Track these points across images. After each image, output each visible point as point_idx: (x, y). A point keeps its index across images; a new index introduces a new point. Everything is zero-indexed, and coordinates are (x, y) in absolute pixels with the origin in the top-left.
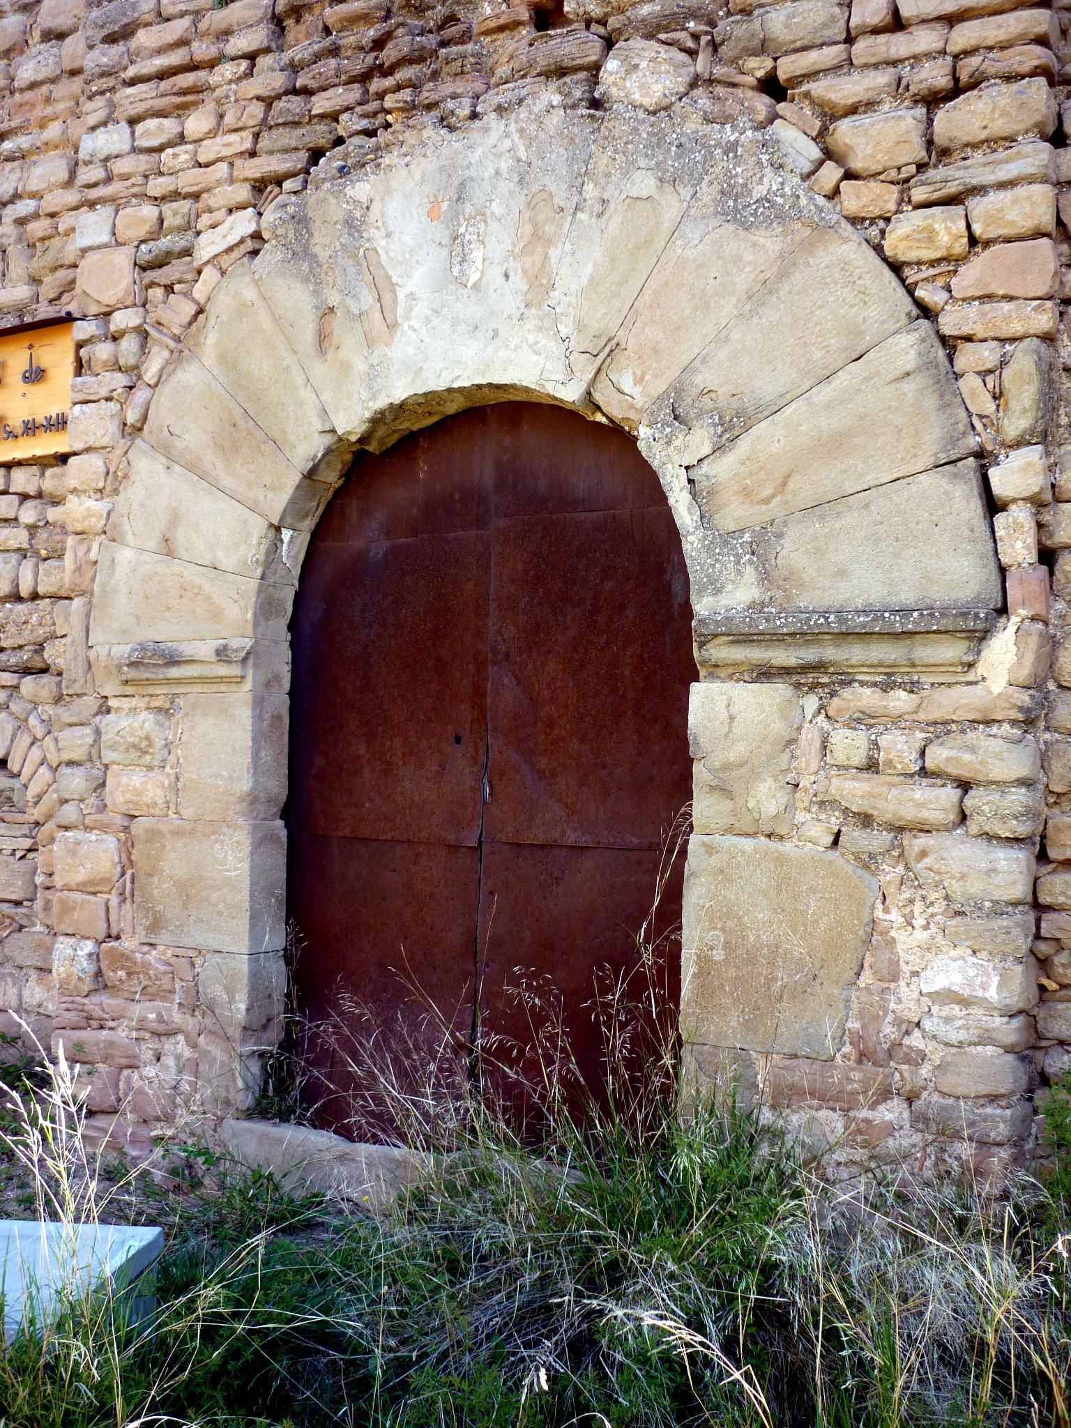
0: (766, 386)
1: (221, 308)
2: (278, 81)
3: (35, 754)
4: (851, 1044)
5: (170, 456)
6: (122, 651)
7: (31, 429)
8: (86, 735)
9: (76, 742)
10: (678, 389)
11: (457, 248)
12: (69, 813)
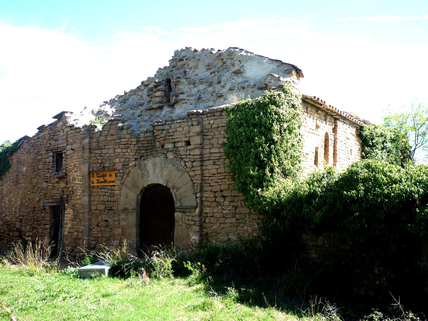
0: (180, 186)
1: (132, 171)
2: (137, 148)
3: (111, 220)
4: (241, 52)
5: (126, 186)
6: (122, 208)
7: (110, 182)
8: (118, 218)
9: (116, 218)
10: (173, 185)
11: (155, 170)
12: (116, 226)
